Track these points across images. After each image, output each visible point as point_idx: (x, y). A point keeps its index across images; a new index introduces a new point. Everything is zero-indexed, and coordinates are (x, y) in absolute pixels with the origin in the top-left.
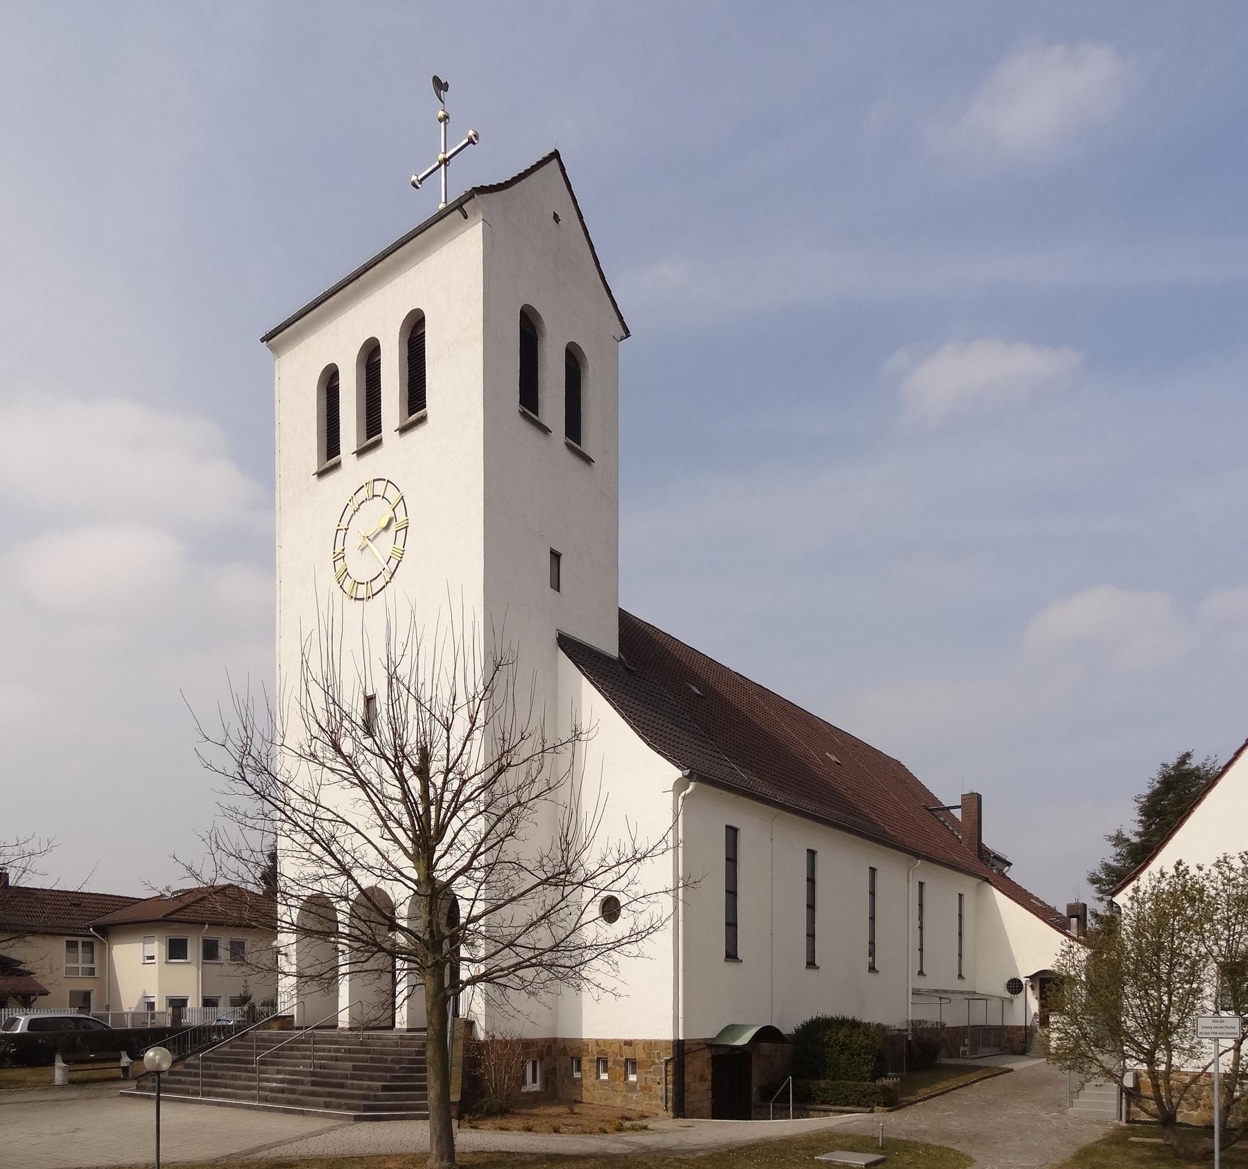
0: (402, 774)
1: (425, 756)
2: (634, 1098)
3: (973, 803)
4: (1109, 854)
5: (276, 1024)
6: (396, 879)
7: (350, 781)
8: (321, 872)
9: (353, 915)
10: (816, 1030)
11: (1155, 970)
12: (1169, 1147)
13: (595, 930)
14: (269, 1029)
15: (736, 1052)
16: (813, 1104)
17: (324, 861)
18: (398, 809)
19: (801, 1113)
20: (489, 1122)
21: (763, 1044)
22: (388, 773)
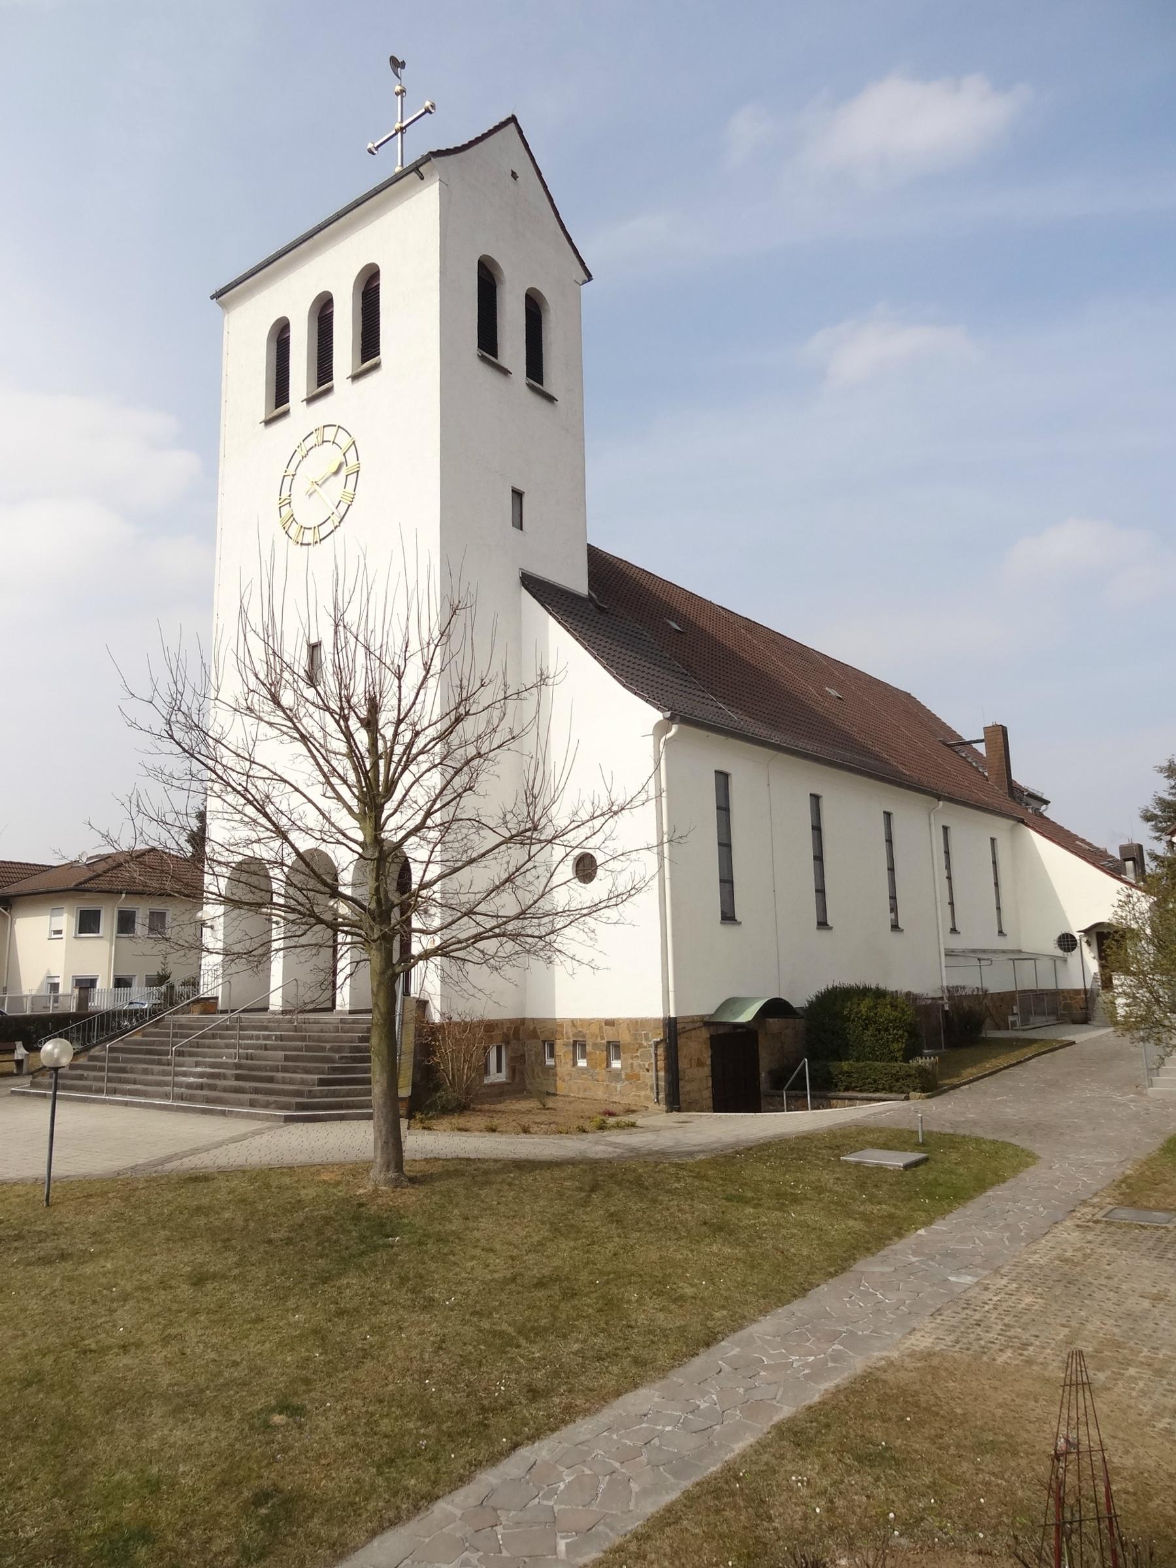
1: (374, 706)
2: (619, 1089)
3: (998, 736)
5: (198, 1007)
6: (338, 842)
15: (739, 1030)
18: (344, 766)
19: (822, 1102)
20: (445, 1122)
22: (332, 726)
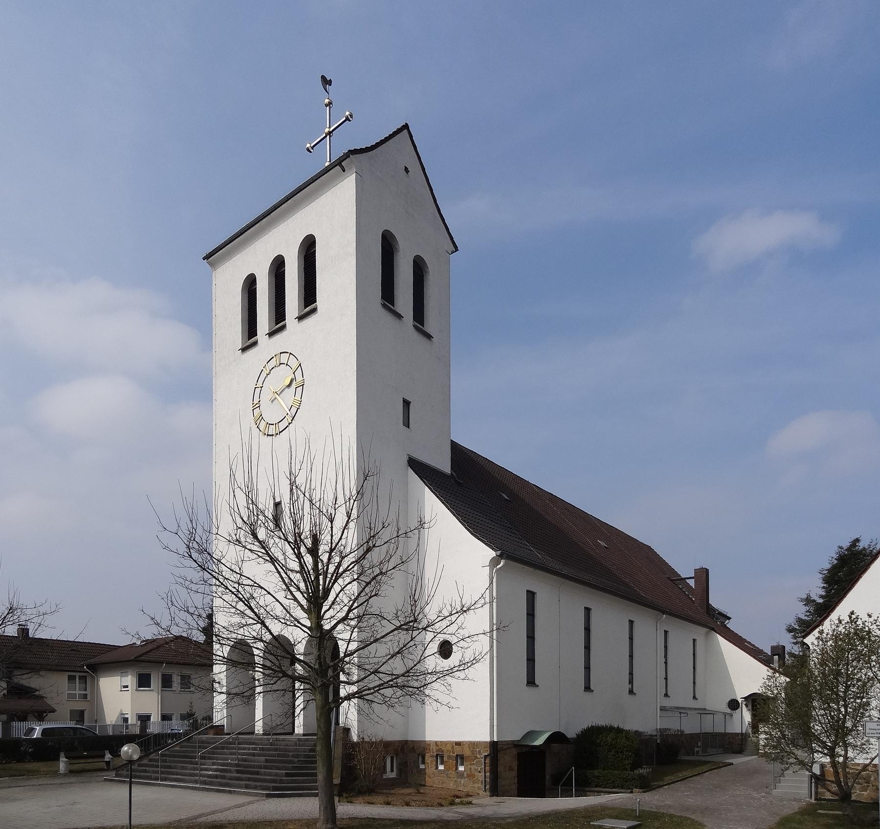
0: (300, 553)
1: (316, 540)
2: (462, 782)
3: (703, 575)
4: (802, 611)
5: (212, 731)
6: (295, 626)
7: (263, 559)
8: (243, 621)
9: (267, 651)
10: (592, 734)
11: (835, 690)
12: (846, 816)
13: (433, 662)
14: (207, 734)
15: (535, 750)
16: (589, 787)
17: (245, 614)
18: (296, 577)
19: (581, 793)
20: (360, 799)
21: (554, 745)
22: (289, 552)
